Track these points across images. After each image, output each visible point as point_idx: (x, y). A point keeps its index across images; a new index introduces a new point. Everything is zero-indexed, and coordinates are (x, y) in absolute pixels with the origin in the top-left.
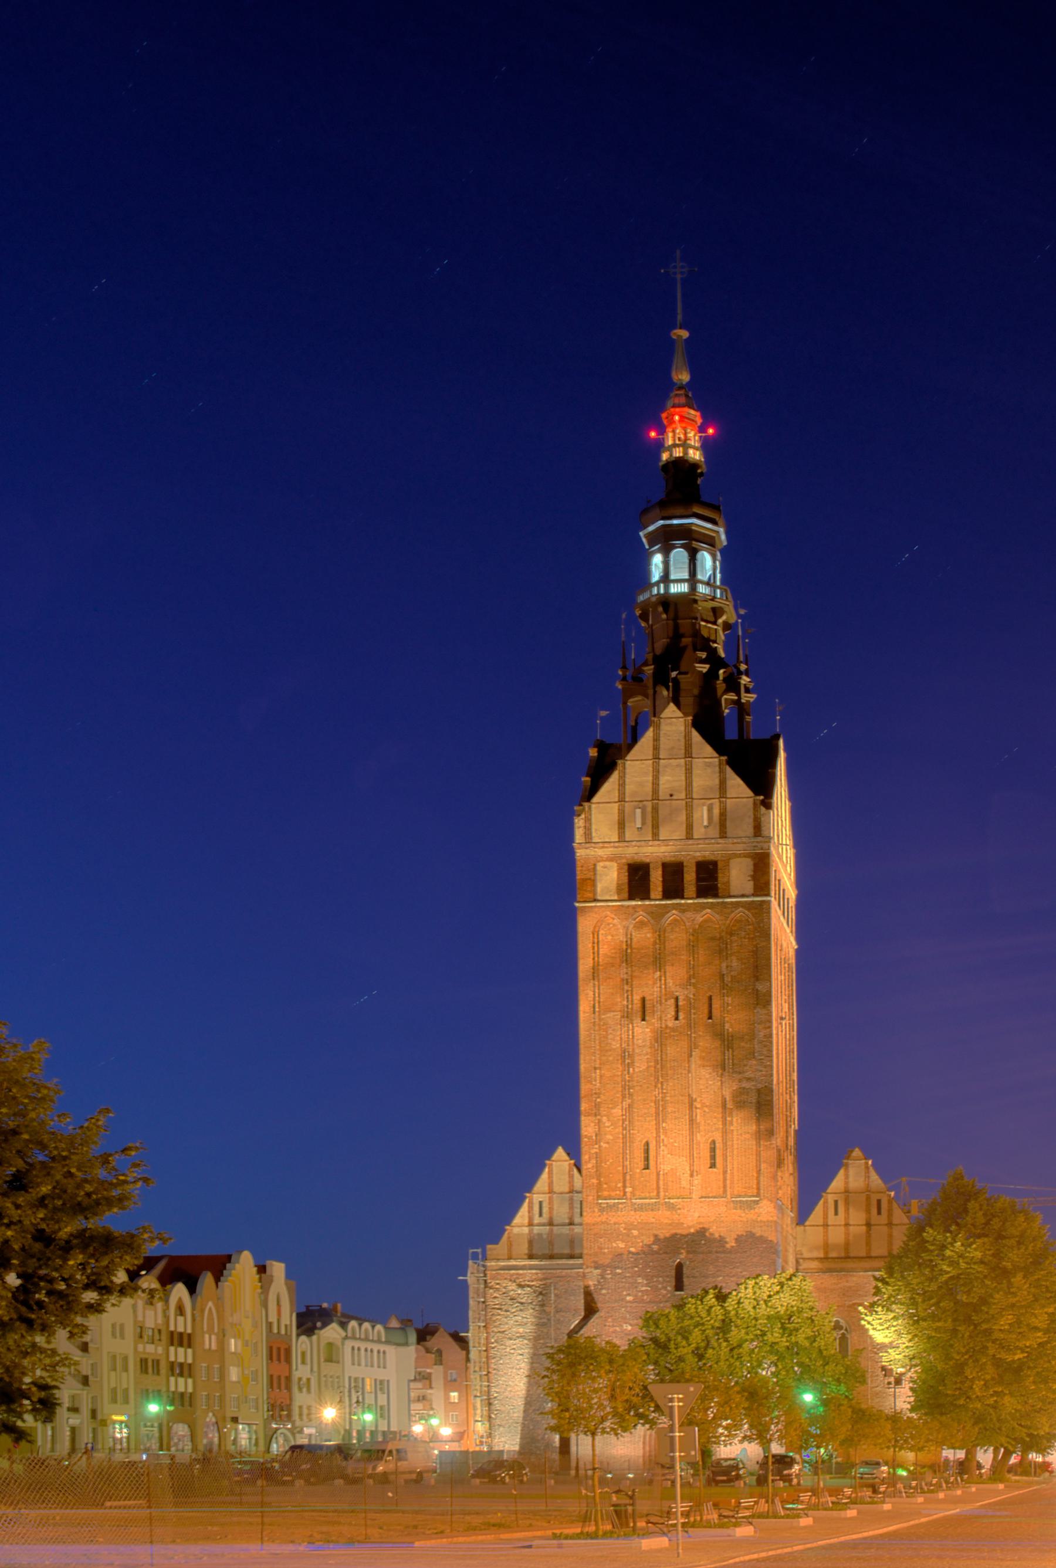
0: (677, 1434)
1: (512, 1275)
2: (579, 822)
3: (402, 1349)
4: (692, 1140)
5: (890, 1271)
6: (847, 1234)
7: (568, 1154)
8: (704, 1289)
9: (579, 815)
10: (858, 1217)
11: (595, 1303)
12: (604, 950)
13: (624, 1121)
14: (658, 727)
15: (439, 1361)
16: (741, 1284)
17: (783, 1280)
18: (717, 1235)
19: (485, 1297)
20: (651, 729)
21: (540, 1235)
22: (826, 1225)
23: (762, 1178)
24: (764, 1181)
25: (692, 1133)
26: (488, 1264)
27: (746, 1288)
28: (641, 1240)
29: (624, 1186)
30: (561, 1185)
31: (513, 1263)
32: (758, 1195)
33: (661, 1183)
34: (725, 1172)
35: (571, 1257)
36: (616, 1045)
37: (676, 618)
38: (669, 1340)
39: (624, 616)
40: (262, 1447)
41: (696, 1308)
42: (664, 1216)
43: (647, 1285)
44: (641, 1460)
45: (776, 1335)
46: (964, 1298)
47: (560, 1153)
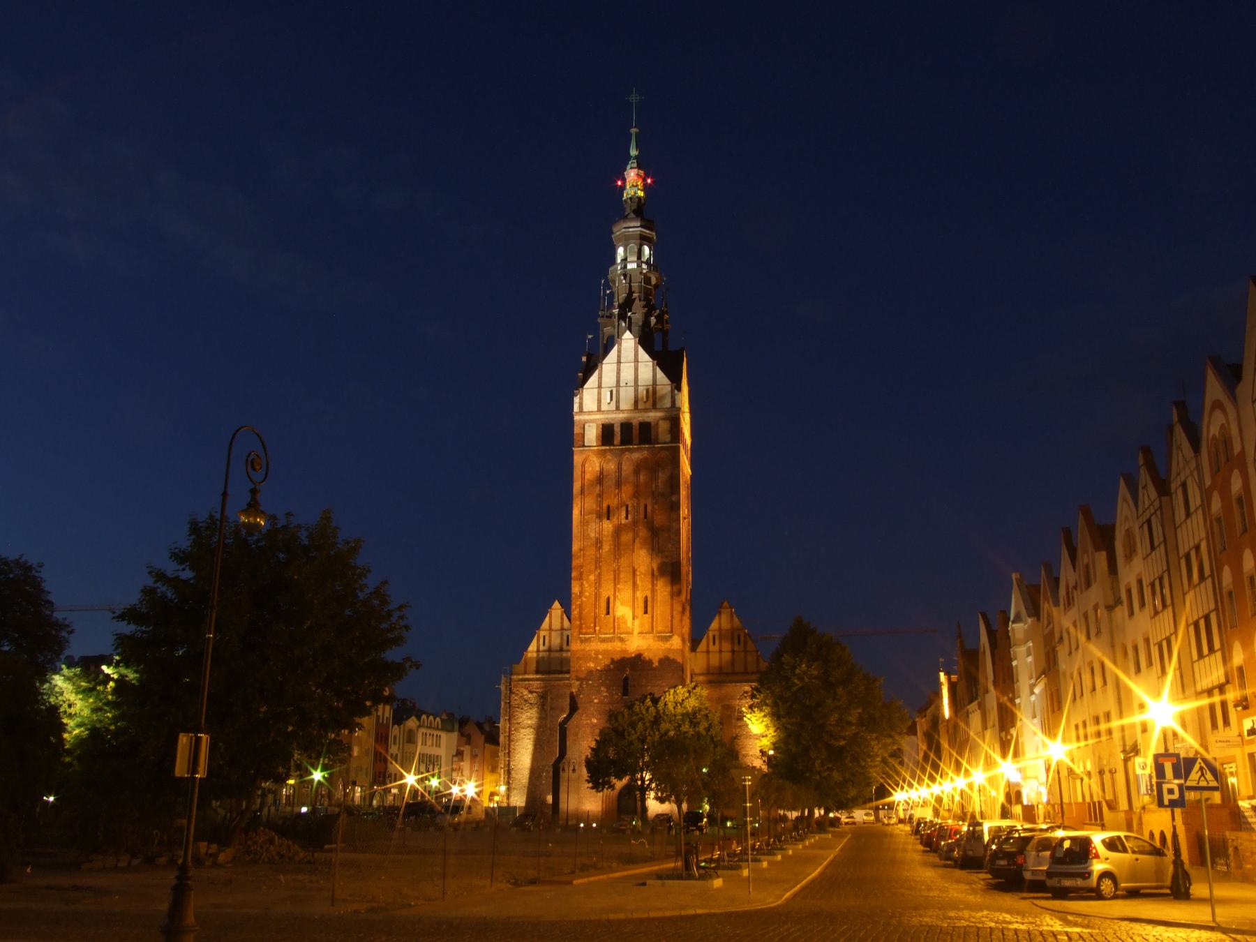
0: (748, 805)
1: (526, 685)
2: (576, 400)
3: (451, 735)
4: (634, 596)
5: (760, 681)
6: (720, 658)
7: (561, 605)
8: (644, 695)
9: (576, 396)
10: (726, 646)
11: (576, 704)
12: (588, 476)
13: (596, 583)
14: (620, 345)
15: (468, 743)
16: (666, 692)
17: (690, 689)
18: (647, 658)
19: (509, 700)
20: (617, 345)
21: (543, 658)
22: (708, 652)
23: (674, 621)
24: (676, 622)
25: (634, 592)
26: (514, 677)
27: (669, 695)
28: (604, 661)
29: (595, 626)
30: (556, 625)
31: (527, 676)
32: (672, 632)
33: (616, 624)
34: (653, 617)
35: (561, 672)
36: (592, 535)
37: (630, 283)
38: (624, 730)
39: (603, 282)
40: (367, 803)
41: (640, 708)
42: (617, 645)
43: (607, 692)
44: (600, 814)
45: (687, 726)
46: (808, 703)
47: (557, 604)
